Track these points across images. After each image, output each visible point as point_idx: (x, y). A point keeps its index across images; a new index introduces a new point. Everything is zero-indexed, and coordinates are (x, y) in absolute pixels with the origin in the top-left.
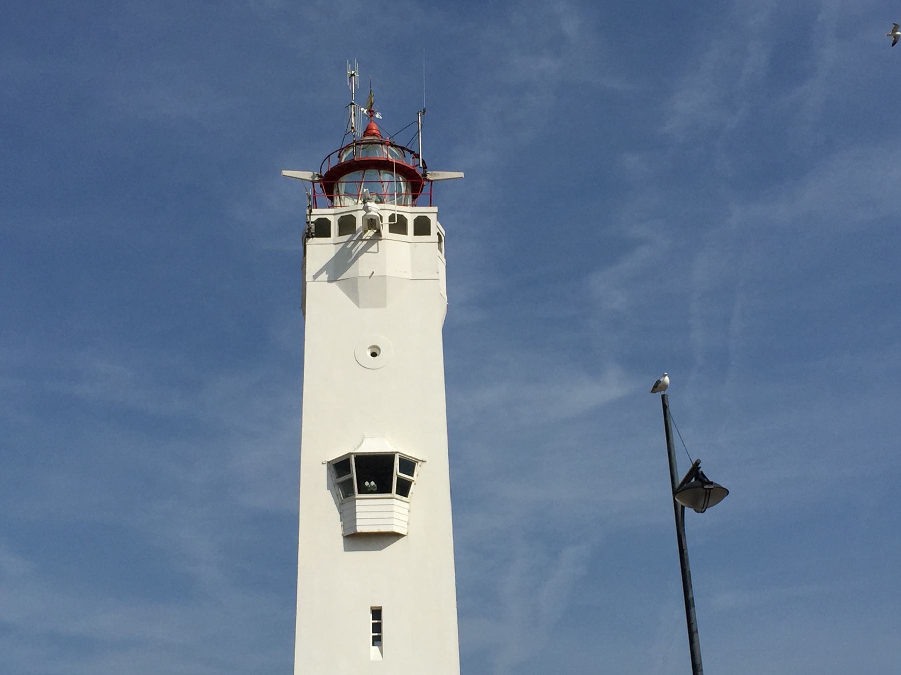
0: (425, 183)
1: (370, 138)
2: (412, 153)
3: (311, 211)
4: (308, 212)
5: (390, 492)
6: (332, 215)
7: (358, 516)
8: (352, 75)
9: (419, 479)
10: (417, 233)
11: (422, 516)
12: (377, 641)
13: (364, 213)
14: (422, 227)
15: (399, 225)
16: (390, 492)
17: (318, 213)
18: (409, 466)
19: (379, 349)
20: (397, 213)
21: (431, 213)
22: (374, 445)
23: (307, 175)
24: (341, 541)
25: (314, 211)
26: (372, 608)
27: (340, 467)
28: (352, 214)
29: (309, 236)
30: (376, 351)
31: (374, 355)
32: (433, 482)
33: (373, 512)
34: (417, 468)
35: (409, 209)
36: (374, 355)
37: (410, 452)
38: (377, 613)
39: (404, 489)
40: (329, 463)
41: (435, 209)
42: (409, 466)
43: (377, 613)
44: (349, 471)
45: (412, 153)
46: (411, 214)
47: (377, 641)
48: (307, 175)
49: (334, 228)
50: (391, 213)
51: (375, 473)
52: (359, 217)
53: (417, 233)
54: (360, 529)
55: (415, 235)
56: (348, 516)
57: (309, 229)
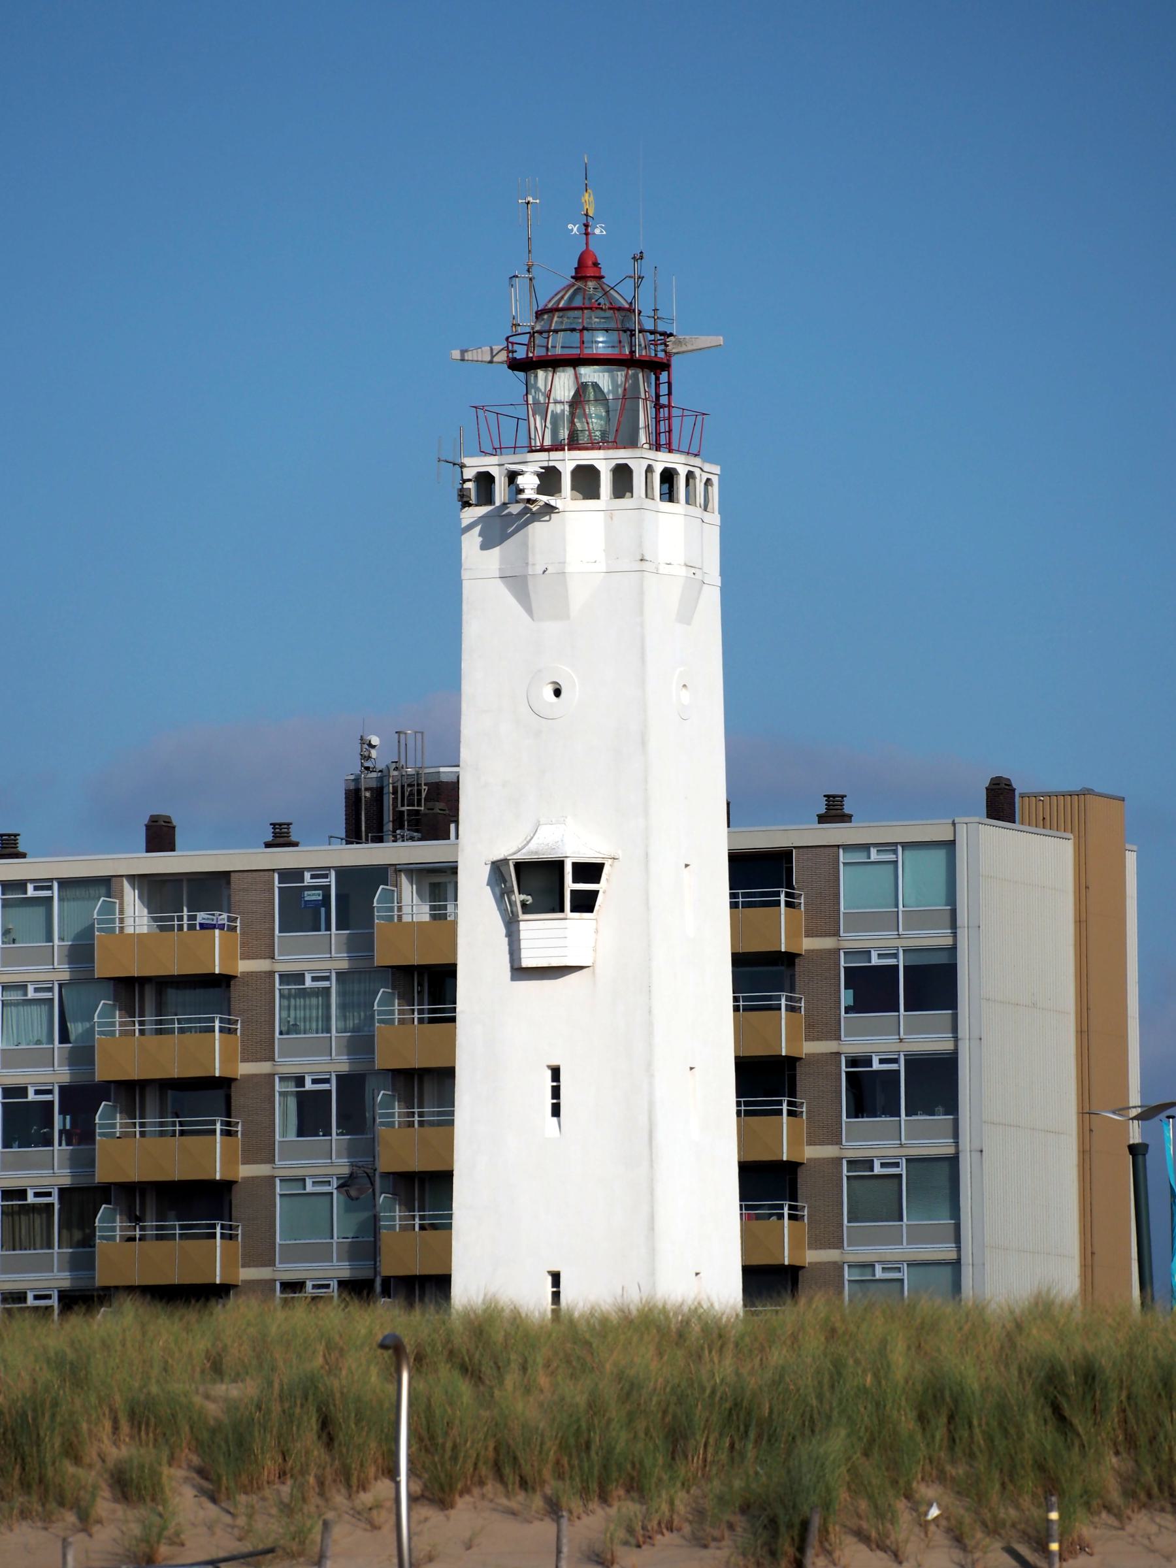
12: (556, 1111)
16: (562, 910)
31: (557, 693)
33: (548, 936)
34: (555, 1119)
38: (556, 1073)
47: (556, 1111)
54: (526, 963)
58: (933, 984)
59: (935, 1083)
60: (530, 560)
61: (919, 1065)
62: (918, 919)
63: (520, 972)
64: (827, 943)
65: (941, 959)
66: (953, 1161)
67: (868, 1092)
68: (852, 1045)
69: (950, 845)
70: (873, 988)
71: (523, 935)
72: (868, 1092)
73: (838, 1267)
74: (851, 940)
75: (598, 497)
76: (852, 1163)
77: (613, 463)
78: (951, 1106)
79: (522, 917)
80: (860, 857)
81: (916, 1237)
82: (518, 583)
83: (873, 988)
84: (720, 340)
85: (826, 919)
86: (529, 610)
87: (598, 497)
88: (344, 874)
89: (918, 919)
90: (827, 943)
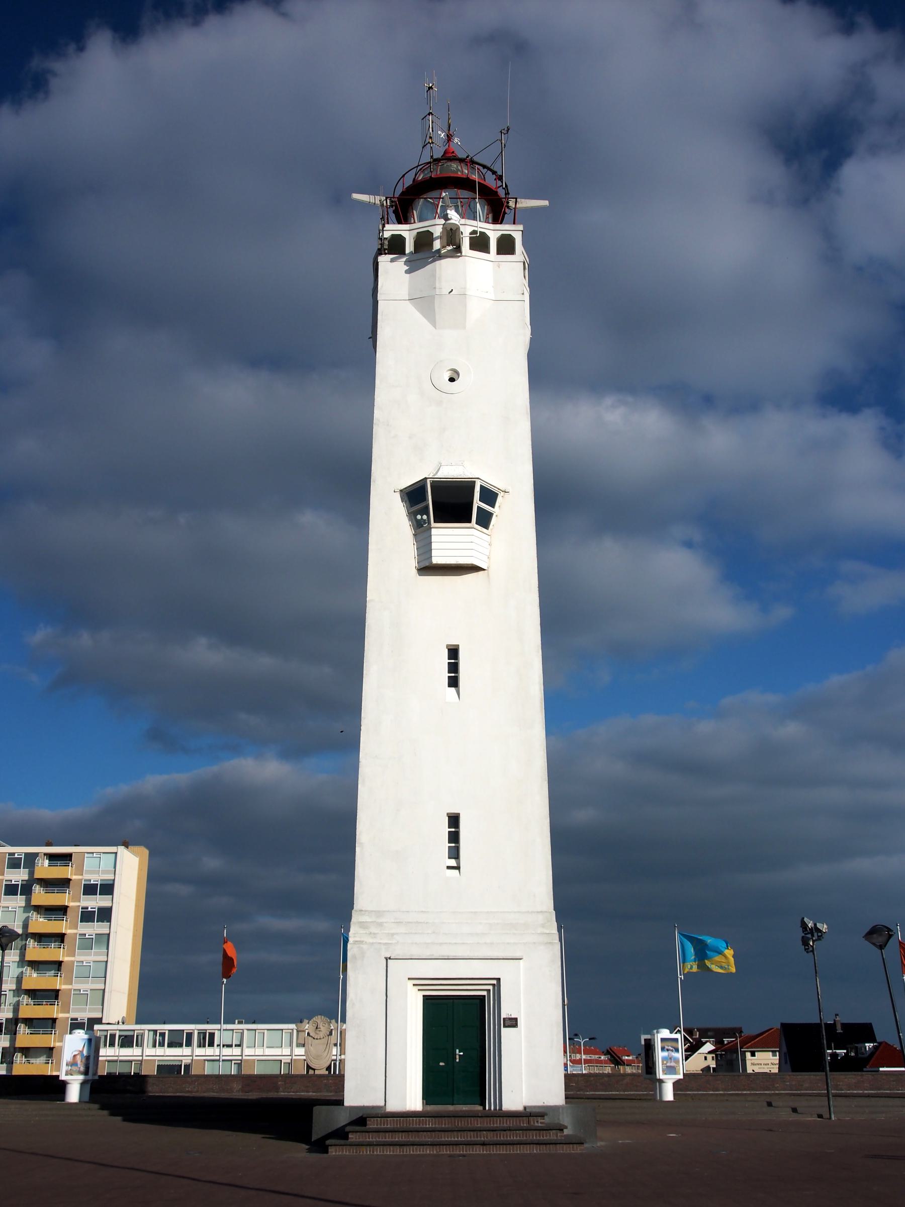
0: (507, 211)
1: (449, 156)
2: (494, 173)
3: (384, 226)
4: (381, 227)
5: (470, 521)
6: (408, 232)
7: (434, 546)
8: (430, 88)
9: (498, 511)
10: (499, 252)
11: (507, 546)
12: (454, 682)
13: (442, 221)
14: (506, 246)
15: (480, 243)
16: (470, 521)
17: (392, 229)
18: (490, 496)
19: (458, 374)
20: (480, 230)
21: (516, 232)
22: (451, 471)
23: (377, 200)
24: (415, 571)
25: (387, 227)
26: (447, 646)
27: (414, 496)
28: (430, 229)
29: (380, 252)
30: (455, 376)
31: (452, 380)
32: (516, 512)
33: (451, 541)
34: (453, 689)
35: (491, 226)
36: (452, 380)
37: (493, 480)
38: (453, 652)
39: (485, 520)
40: (401, 491)
41: (521, 227)
42: (490, 496)
43: (453, 652)
44: (424, 499)
45: (494, 173)
46: (494, 232)
47: (454, 682)
48: (377, 200)
49: (409, 247)
50: (471, 229)
51: (450, 502)
52: (437, 231)
53: (499, 252)
54: (436, 560)
55: (498, 253)
56: (424, 545)
57: (382, 245)
58: (108, 889)
59: (105, 914)
60: (437, 285)
61: (101, 910)
62: (104, 872)
63: (428, 569)
64: (80, 877)
65: (111, 882)
66: (109, 935)
67: (87, 916)
68: (83, 903)
69: (116, 853)
70: (90, 889)
71: (434, 539)
72: (87, 916)
73: (73, 962)
74: (86, 876)
75: (489, 253)
76: (80, 935)
77: (499, 233)
78: (109, 920)
79: (433, 524)
80: (91, 855)
81: (96, 954)
82: (425, 303)
83: (90, 889)
84: (356, 196)
85: (80, 871)
86: (433, 323)
87: (489, 253)
88: (26, 854)
89: (104, 872)
90: (80, 877)
